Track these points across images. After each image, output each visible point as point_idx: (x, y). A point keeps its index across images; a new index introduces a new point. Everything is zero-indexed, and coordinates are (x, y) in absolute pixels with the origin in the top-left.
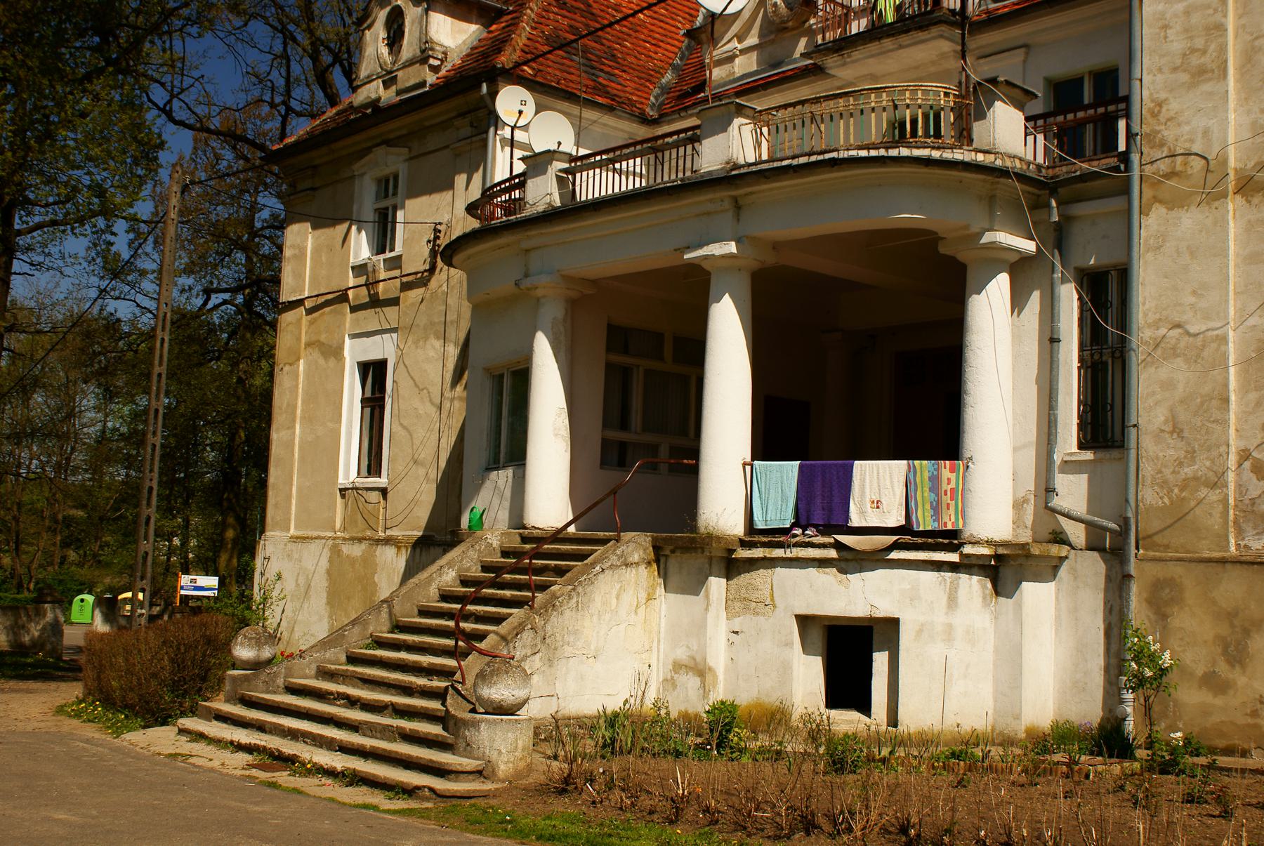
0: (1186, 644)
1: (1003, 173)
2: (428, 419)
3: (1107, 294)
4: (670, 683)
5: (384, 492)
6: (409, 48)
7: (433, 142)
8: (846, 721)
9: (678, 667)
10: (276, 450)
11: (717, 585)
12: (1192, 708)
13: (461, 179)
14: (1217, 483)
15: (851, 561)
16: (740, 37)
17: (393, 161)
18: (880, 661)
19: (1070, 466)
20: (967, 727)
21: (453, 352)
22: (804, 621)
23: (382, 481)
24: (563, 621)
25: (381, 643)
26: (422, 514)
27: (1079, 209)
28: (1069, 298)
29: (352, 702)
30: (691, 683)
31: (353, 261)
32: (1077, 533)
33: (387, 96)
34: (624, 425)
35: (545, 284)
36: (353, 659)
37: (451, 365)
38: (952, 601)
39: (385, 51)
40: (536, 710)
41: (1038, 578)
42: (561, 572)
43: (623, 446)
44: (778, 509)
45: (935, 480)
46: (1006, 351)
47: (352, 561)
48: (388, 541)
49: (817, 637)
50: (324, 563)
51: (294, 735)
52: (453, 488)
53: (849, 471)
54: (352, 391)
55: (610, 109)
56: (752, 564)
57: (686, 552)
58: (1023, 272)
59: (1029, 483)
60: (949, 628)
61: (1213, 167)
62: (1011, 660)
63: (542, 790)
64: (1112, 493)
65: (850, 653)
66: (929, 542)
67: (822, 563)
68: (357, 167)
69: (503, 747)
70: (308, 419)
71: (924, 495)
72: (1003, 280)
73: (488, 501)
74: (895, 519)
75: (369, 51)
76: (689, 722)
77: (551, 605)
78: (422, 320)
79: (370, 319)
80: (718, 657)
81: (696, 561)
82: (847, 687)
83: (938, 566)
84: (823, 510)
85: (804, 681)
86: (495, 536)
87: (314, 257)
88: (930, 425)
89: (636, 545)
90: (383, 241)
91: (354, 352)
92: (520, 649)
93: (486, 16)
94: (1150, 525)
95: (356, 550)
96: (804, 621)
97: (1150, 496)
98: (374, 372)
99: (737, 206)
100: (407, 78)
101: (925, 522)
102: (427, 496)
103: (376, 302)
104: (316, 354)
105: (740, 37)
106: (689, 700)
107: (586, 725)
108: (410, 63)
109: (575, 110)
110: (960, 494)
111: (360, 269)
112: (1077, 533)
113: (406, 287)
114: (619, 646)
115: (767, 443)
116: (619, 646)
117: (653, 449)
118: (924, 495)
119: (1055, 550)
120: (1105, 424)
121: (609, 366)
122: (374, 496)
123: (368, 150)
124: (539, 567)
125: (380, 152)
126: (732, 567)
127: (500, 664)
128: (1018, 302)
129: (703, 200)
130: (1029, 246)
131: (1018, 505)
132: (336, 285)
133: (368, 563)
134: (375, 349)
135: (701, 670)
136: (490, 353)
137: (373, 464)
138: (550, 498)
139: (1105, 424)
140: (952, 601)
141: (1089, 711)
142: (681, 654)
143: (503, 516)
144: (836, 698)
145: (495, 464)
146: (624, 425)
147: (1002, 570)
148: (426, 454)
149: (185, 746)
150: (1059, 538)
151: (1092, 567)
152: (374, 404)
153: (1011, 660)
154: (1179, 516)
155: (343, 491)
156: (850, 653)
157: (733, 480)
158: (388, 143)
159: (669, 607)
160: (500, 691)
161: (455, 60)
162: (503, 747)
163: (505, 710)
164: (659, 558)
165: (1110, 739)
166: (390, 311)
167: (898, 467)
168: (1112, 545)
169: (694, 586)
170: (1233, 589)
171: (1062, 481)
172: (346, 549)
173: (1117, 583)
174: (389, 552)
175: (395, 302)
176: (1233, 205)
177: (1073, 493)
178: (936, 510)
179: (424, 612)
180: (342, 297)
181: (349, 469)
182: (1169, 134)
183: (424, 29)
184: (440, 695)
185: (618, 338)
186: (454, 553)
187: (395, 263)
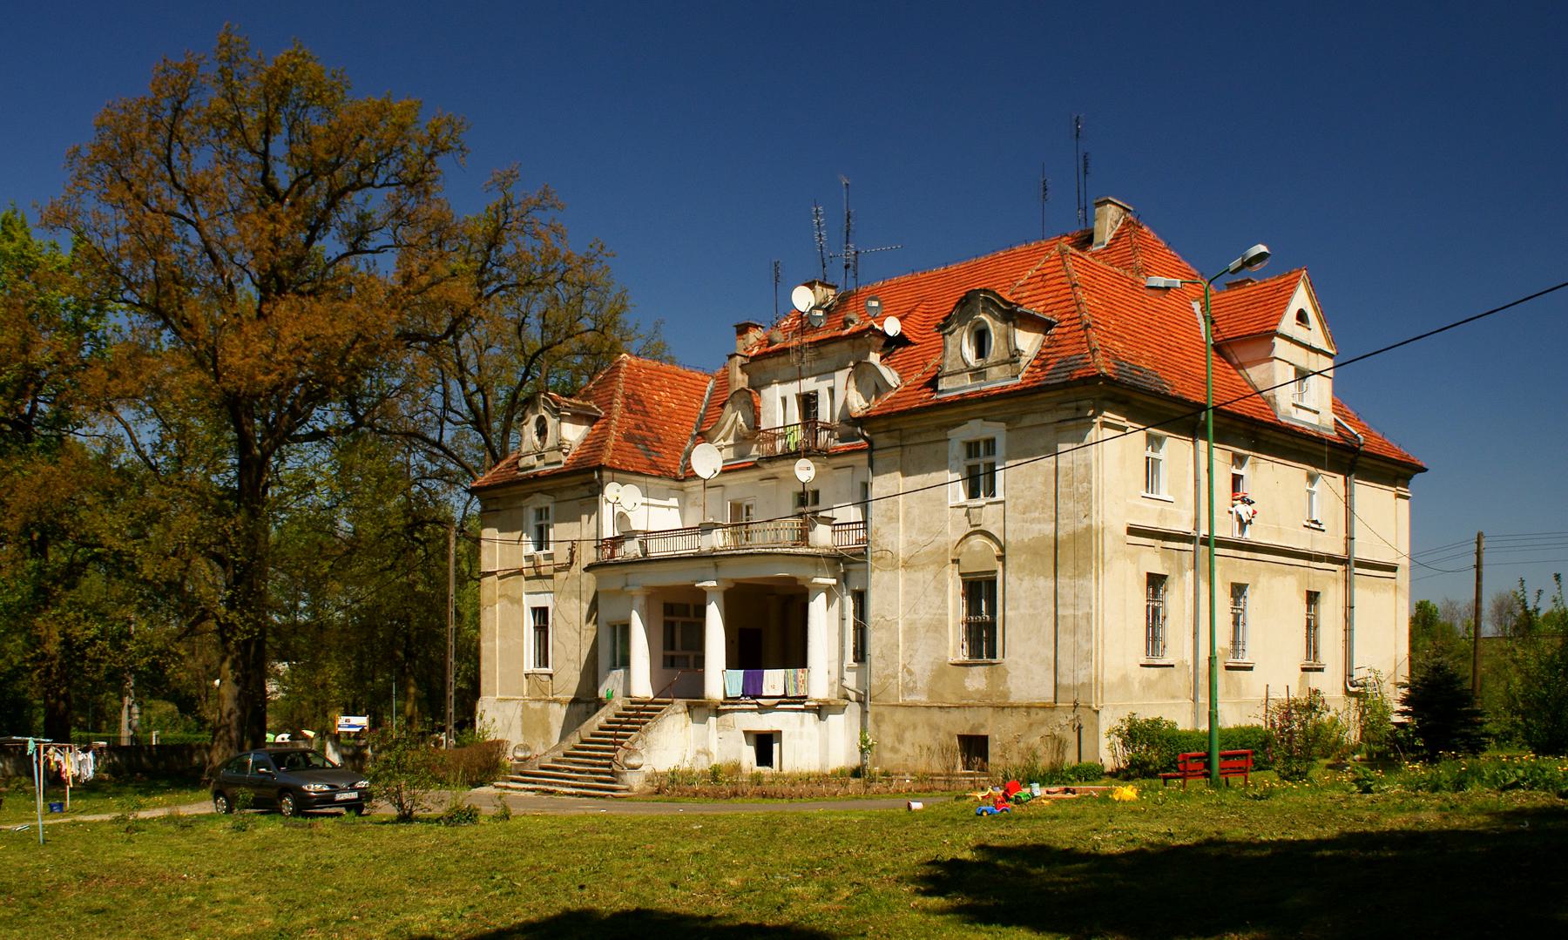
0: (887, 735)
1: (817, 556)
2: (573, 639)
3: (860, 598)
4: (696, 759)
5: (551, 676)
6: (551, 441)
7: (568, 495)
8: (765, 770)
9: (698, 752)
10: (484, 653)
11: (712, 720)
12: (890, 759)
13: (585, 517)
14: (896, 677)
15: (763, 709)
16: (725, 439)
17: (545, 501)
18: (776, 746)
19: (849, 669)
20: (806, 770)
21: (586, 607)
22: (746, 733)
23: (549, 670)
24: (650, 737)
25: (577, 748)
26: (573, 687)
27: (852, 567)
28: (849, 602)
29: (571, 771)
30: (703, 759)
31: (525, 553)
32: (853, 696)
33: (541, 467)
34: (673, 648)
35: (634, 590)
36: (566, 755)
37: (585, 613)
38: (802, 723)
39: (536, 438)
40: (646, 769)
41: (836, 713)
42: (651, 717)
43: (673, 658)
44: (736, 690)
45: (796, 677)
46: (825, 623)
47: (535, 711)
48: (555, 701)
49: (752, 739)
50: (519, 712)
51: (550, 784)
52: (591, 675)
53: (762, 675)
54: (529, 623)
55: (659, 477)
56: (726, 711)
57: (700, 707)
58: (829, 590)
59: (835, 676)
60: (801, 734)
61: (894, 556)
62: (825, 745)
63: (651, 794)
64: (862, 680)
65: (764, 744)
66: (793, 701)
67: (752, 710)
68: (525, 502)
69: (635, 781)
70: (503, 637)
71: (791, 683)
72: (823, 596)
73: (610, 685)
74: (781, 693)
75: (527, 437)
76: (704, 774)
77: (648, 730)
78: (567, 588)
79: (537, 585)
80: (714, 747)
81: (704, 711)
82: (764, 757)
83: (796, 710)
84: (752, 690)
85: (748, 755)
86: (619, 702)
87: (501, 550)
88: (795, 655)
89: (680, 704)
90: (541, 543)
91: (529, 602)
92: (638, 745)
93: (591, 420)
94: (875, 692)
95: (538, 706)
96: (746, 733)
97: (874, 681)
98: (541, 614)
99: (716, 566)
100: (552, 457)
101: (792, 693)
102: (575, 679)
103: (539, 576)
104: (505, 602)
105: (725, 439)
106: (703, 765)
107: (664, 775)
108: (552, 449)
109: (642, 479)
110: (806, 682)
111: (529, 558)
112: (853, 696)
113: (556, 570)
114: (675, 745)
115: (731, 664)
116: (675, 745)
117: (687, 658)
118: (791, 683)
119: (842, 702)
120: (861, 654)
121: (665, 622)
122: (546, 678)
123: (530, 495)
124: (639, 716)
125: (538, 496)
126: (718, 713)
127: (631, 752)
128: (829, 603)
129: (703, 563)
130: (834, 581)
131: (831, 684)
132: (515, 565)
133: (544, 712)
134: (541, 601)
135: (707, 753)
136: (608, 613)
137: (543, 660)
138: (642, 683)
139: (861, 654)
140: (802, 723)
141: (856, 761)
142: (700, 748)
143: (619, 691)
144: (760, 763)
145: (614, 667)
146: (673, 648)
147: (821, 710)
148: (574, 656)
149: (498, 791)
150: (846, 697)
151: (855, 708)
152: (542, 629)
153: (825, 745)
154: (884, 690)
155: (527, 675)
156: (764, 744)
157: (719, 678)
158: (542, 492)
159: (694, 729)
160: (633, 761)
161: (576, 448)
162: (635, 781)
163: (634, 768)
164: (690, 709)
165: (857, 773)
166: (549, 582)
167: (782, 671)
168: (861, 701)
169: (704, 721)
170: (900, 715)
171: (847, 675)
172: (531, 705)
173: (864, 713)
174: (557, 706)
175: (551, 577)
176: (901, 572)
177: (851, 680)
178: (797, 689)
179: (593, 735)
180: (520, 572)
181: (529, 663)
182: (880, 541)
183: (559, 432)
184: (610, 766)
185: (669, 609)
186: (602, 710)
187: (550, 557)
